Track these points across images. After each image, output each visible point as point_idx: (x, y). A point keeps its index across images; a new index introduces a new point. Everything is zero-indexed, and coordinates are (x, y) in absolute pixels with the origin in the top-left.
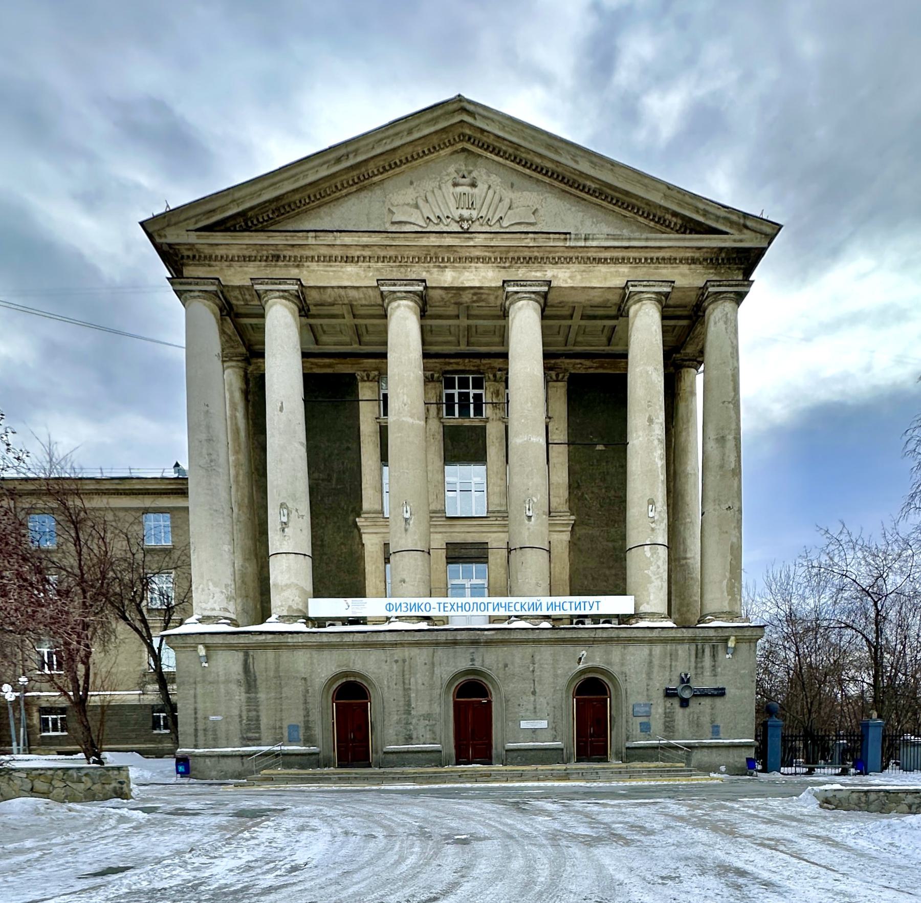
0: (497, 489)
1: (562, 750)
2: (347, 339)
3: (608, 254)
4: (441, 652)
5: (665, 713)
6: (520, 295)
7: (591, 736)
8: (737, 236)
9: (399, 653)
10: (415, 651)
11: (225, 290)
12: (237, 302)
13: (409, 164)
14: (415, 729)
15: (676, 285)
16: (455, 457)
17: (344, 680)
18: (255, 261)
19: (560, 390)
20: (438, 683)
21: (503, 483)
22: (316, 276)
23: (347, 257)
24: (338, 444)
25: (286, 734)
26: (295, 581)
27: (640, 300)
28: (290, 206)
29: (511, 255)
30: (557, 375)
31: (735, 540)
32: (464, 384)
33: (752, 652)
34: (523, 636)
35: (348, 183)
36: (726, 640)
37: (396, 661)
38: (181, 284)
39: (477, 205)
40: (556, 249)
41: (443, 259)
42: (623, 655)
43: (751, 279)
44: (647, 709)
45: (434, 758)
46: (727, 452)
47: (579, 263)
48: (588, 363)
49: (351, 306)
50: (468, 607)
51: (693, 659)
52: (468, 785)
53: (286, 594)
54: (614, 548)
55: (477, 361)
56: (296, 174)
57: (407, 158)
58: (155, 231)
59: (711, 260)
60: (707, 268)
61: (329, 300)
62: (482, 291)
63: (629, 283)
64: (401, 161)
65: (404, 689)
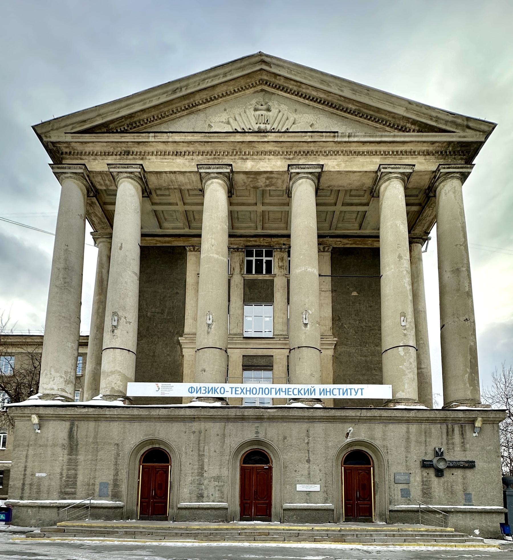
0: (281, 320)
1: (333, 510)
2: (181, 225)
3: (365, 148)
4: (231, 426)
5: (423, 481)
6: (300, 175)
7: (154, 498)
8: (462, 134)
9: (196, 426)
10: (209, 425)
11: (91, 175)
12: (100, 184)
13: (224, 98)
14: (206, 489)
15: (416, 168)
16: (251, 299)
17: (150, 447)
18: (112, 155)
19: (327, 256)
20: (227, 451)
21: (285, 316)
22: (153, 164)
23: (177, 152)
24: (170, 290)
25: (97, 490)
26: (119, 370)
27: (389, 179)
28: (140, 122)
29: (294, 149)
30: (324, 248)
31: (472, 344)
32: (259, 254)
33: (496, 432)
34: (300, 413)
35: (181, 108)
36: (473, 422)
37: (194, 432)
38: (58, 168)
39: (271, 121)
40: (328, 144)
41: (245, 153)
42: (384, 432)
43: (473, 163)
44: (407, 477)
45: (222, 515)
46: (462, 279)
47: (344, 155)
48: (345, 241)
49: (181, 190)
50: (258, 390)
51: (445, 436)
52: (246, 544)
53: (110, 378)
54: (366, 361)
55: (269, 239)
56: (145, 99)
57: (223, 94)
58: (42, 133)
59: (441, 152)
60: (438, 159)
61: (164, 185)
62: (272, 175)
63: (381, 166)
64: (218, 96)
65: (199, 455)
